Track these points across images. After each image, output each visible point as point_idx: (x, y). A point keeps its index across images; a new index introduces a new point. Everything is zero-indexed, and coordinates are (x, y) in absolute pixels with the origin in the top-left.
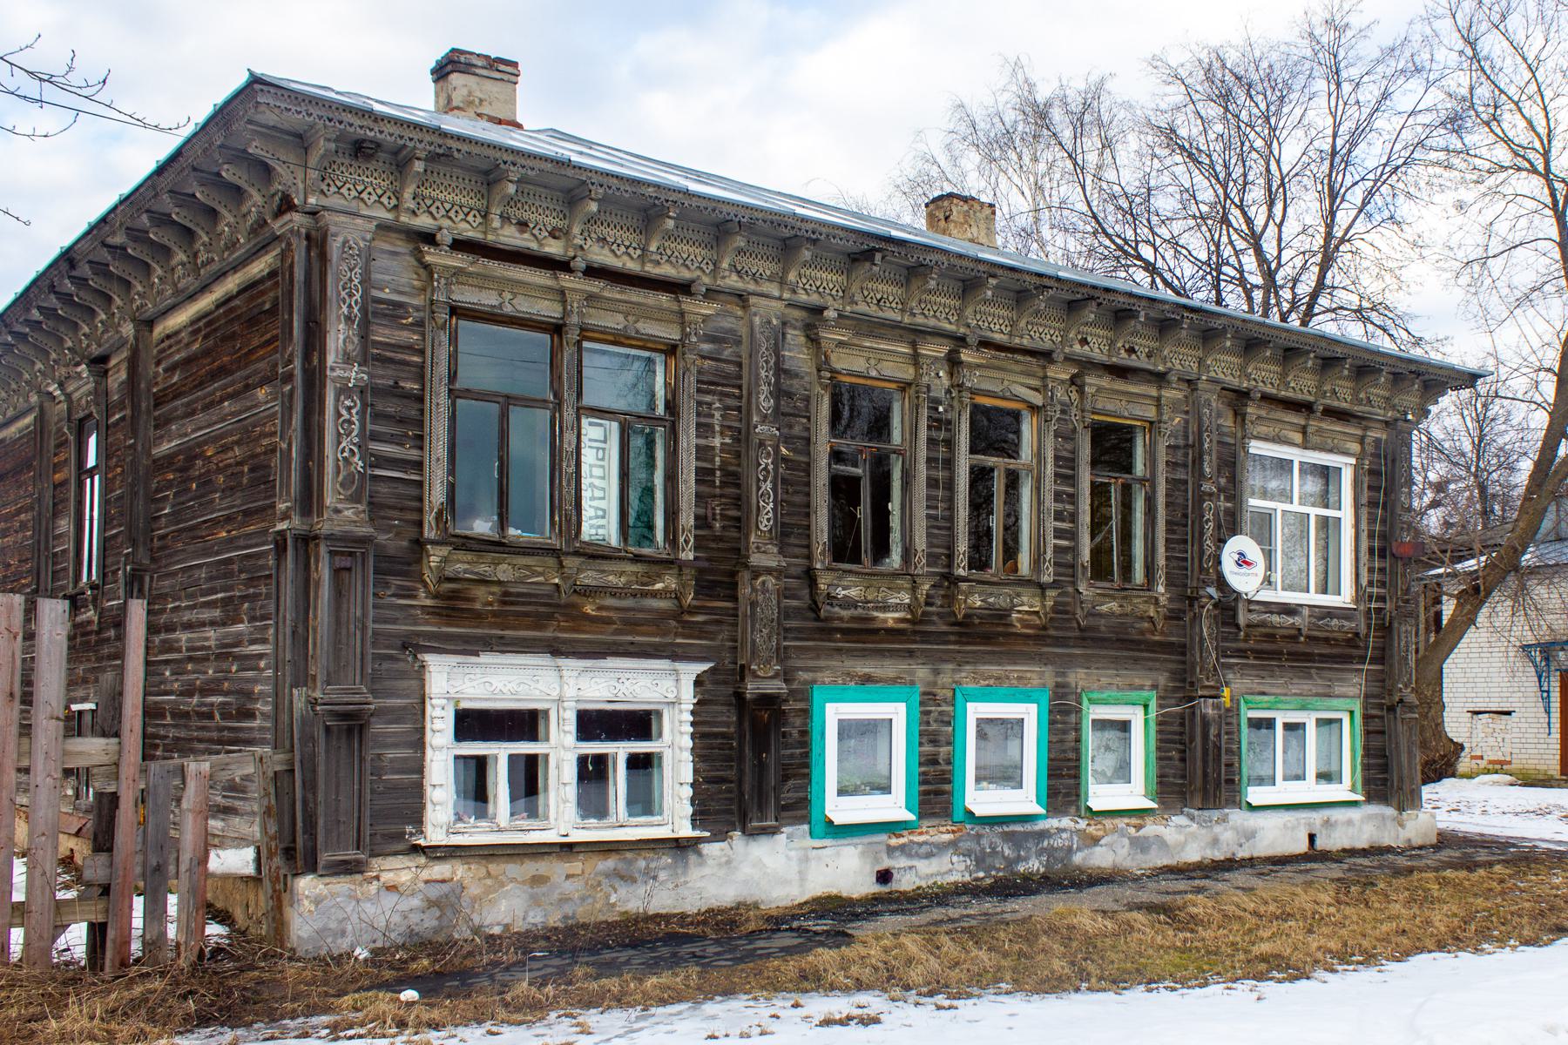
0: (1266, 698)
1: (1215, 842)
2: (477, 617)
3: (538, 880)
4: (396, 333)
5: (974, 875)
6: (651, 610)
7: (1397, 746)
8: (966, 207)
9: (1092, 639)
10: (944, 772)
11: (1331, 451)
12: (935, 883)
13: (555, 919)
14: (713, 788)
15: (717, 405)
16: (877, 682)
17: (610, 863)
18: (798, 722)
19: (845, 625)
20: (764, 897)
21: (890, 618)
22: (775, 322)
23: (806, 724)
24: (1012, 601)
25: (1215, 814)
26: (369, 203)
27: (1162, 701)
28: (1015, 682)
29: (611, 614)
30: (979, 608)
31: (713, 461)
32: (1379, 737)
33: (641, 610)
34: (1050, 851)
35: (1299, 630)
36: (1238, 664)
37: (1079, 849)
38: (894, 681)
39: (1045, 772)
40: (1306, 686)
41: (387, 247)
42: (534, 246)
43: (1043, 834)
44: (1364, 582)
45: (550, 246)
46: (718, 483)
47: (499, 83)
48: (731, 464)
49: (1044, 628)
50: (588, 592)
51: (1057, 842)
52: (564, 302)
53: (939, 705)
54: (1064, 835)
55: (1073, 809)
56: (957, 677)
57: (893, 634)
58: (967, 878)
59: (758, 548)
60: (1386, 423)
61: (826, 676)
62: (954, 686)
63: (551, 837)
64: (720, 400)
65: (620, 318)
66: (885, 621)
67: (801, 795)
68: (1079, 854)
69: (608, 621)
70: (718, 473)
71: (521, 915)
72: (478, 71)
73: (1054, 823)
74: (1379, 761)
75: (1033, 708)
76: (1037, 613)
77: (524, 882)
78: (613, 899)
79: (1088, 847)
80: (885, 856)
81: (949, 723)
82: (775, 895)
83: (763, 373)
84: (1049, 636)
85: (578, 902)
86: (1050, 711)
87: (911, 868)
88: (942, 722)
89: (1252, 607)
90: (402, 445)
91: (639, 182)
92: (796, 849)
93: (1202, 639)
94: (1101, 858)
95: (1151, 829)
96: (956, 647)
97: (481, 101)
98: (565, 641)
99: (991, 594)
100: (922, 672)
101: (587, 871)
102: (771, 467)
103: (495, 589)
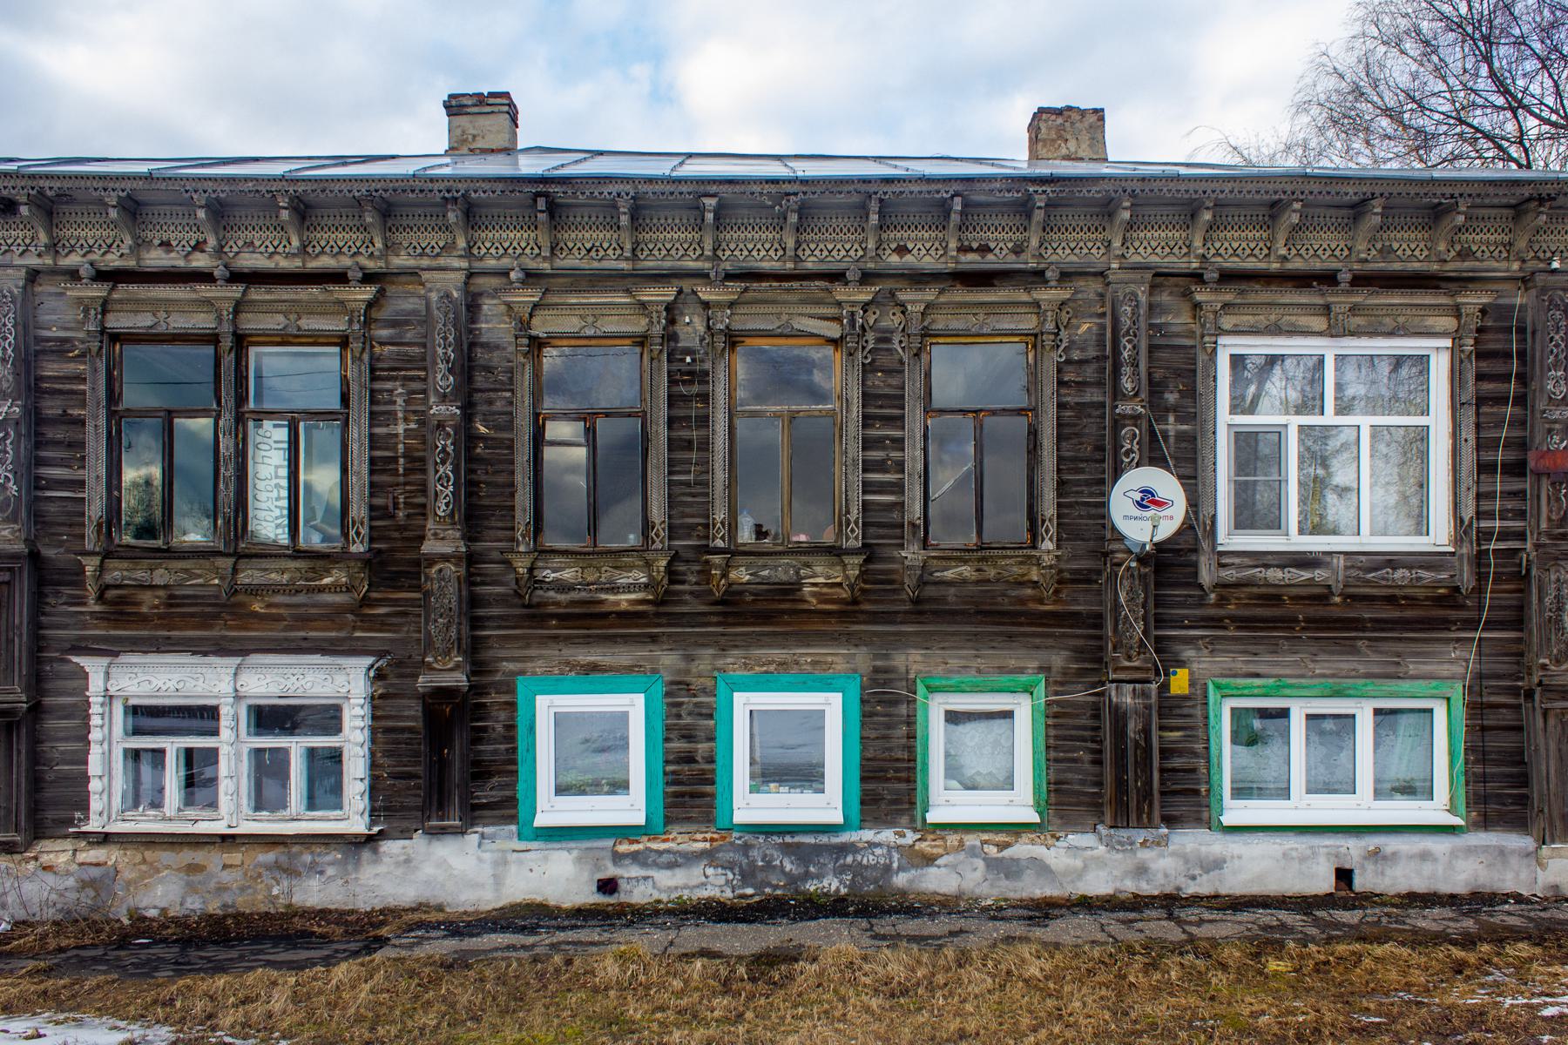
0: (1257, 681)
1: (1141, 871)
2: (143, 620)
3: (193, 868)
4: (65, 366)
5: (738, 892)
6: (327, 605)
7: (1536, 750)
8: (1060, 121)
9: (935, 613)
10: (703, 772)
11: (1391, 334)
12: (680, 897)
13: (214, 907)
14: (400, 783)
15: (400, 390)
16: (606, 671)
17: (269, 857)
18: (503, 715)
19: (562, 610)
20: (449, 899)
21: (624, 600)
22: (455, 294)
23: (513, 718)
24: (797, 573)
25: (1140, 835)
26: (1324, 257)
27: (1058, 682)
28: (808, 667)
29: (282, 611)
30: (748, 583)
31: (395, 449)
32: (1512, 736)
33: (314, 606)
34: (858, 869)
35: (1329, 587)
36: (1202, 637)
37: (900, 869)
38: (629, 669)
39: (856, 774)
40: (1345, 663)
41: (53, 289)
42: (181, 263)
43: (844, 849)
44: (1468, 512)
45: (198, 260)
46: (401, 471)
47: (491, 116)
48: (418, 450)
49: (855, 602)
50: (255, 591)
51: (868, 859)
52: (1458, 316)
53: (695, 696)
54: (878, 851)
55: (905, 820)
56: (720, 663)
57: (626, 617)
58: (729, 894)
59: (435, 534)
60: (1523, 280)
61: (539, 666)
62: (716, 674)
63: (219, 828)
64: (403, 385)
65: (281, 318)
66: (617, 603)
67: (507, 793)
68: (901, 875)
69: (278, 618)
70: (401, 461)
71: (179, 900)
72: (469, 110)
73: (868, 835)
74: (1514, 770)
75: (836, 699)
76: (840, 585)
77: (179, 870)
78: (275, 891)
79: (916, 867)
80: (610, 864)
81: (710, 716)
82: (463, 898)
83: (440, 351)
84: (862, 612)
85: (237, 892)
86: (863, 701)
87: (646, 878)
88: (701, 715)
89: (1225, 560)
90: (70, 467)
91: (234, 179)
92: (492, 851)
93: (1117, 606)
94: (938, 880)
95: (1023, 849)
96: (720, 629)
97: (474, 136)
98: (233, 639)
99: (764, 567)
100: (669, 659)
101: (247, 862)
102: (450, 449)
103: (161, 593)
